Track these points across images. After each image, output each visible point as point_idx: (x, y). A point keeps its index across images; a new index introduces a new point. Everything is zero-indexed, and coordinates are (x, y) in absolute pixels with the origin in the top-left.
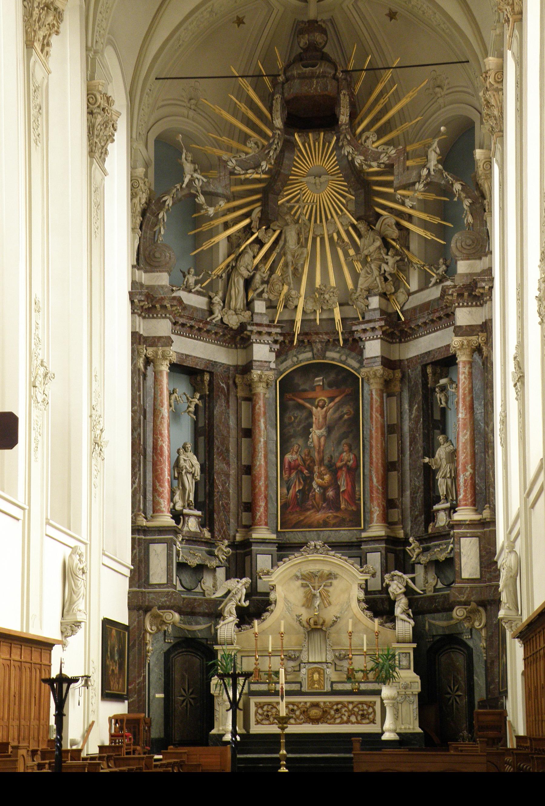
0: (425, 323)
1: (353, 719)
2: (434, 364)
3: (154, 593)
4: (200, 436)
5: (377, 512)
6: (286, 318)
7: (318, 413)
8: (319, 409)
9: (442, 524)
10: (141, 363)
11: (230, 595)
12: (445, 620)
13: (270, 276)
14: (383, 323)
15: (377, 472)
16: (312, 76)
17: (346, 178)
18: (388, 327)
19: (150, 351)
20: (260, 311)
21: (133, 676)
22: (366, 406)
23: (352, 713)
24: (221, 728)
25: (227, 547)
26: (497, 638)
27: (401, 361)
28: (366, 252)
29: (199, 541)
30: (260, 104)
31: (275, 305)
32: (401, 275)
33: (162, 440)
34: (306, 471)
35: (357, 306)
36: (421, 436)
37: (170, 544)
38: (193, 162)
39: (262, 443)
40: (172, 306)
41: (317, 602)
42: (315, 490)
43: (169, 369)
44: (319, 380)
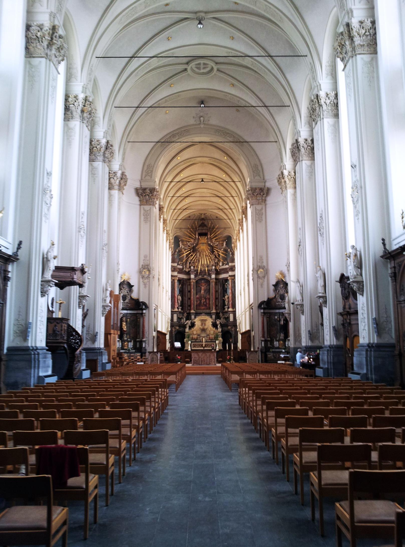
7: (203, 288)
16: (203, 229)
19: (174, 278)
37: (177, 314)
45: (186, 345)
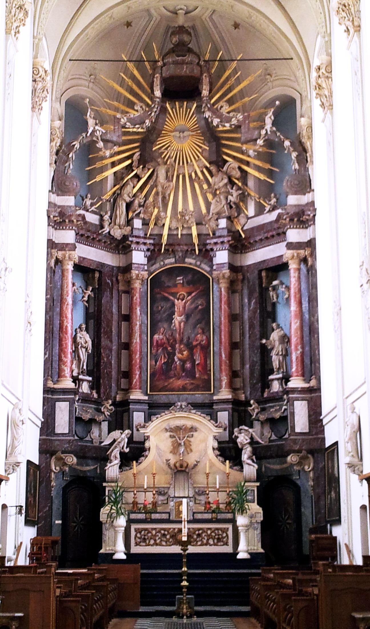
0: (261, 240)
1: (211, 541)
2: (268, 270)
3: (59, 440)
4: (91, 319)
5: (225, 380)
6: (156, 232)
7: (179, 304)
8: (180, 301)
9: (276, 390)
10: (52, 264)
11: (116, 443)
12: (278, 464)
13: (145, 201)
14: (230, 238)
15: (225, 350)
16: (183, 63)
17: (203, 134)
18: (233, 242)
19: (60, 255)
20: (138, 227)
21: (42, 505)
22: (215, 299)
23: (209, 537)
24: (108, 549)
25: (110, 405)
26: (323, 479)
27: (242, 267)
28: (216, 187)
29: (89, 401)
30: (141, 80)
31: (147, 222)
32: (241, 204)
33: (67, 322)
34: (169, 348)
35: (209, 225)
36: (258, 323)
37: (72, 402)
38: (94, 118)
39: (138, 326)
40: (77, 221)
41: (182, 449)
42: (176, 363)
43: (73, 267)
44: (180, 279)
45: (107, 534)
